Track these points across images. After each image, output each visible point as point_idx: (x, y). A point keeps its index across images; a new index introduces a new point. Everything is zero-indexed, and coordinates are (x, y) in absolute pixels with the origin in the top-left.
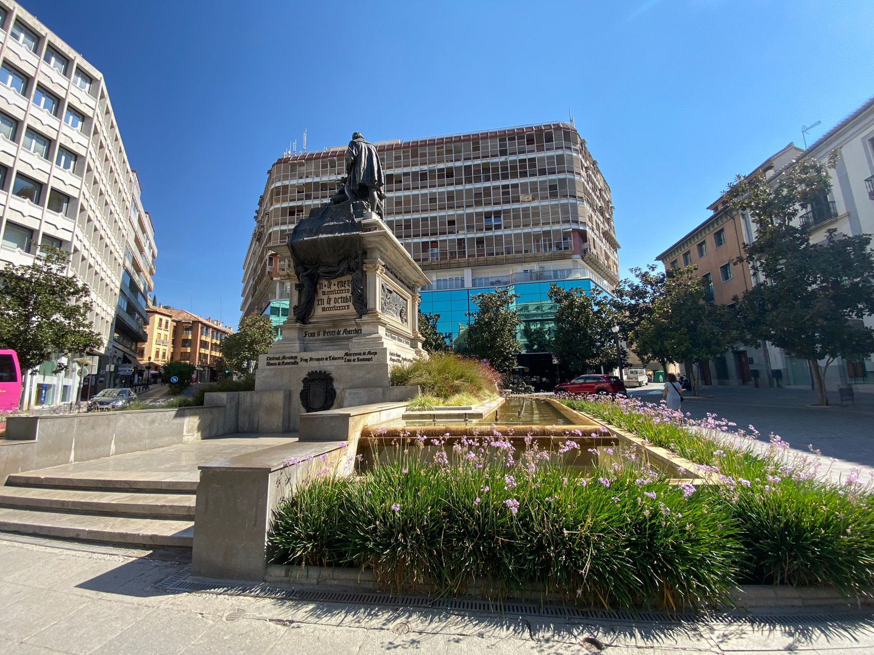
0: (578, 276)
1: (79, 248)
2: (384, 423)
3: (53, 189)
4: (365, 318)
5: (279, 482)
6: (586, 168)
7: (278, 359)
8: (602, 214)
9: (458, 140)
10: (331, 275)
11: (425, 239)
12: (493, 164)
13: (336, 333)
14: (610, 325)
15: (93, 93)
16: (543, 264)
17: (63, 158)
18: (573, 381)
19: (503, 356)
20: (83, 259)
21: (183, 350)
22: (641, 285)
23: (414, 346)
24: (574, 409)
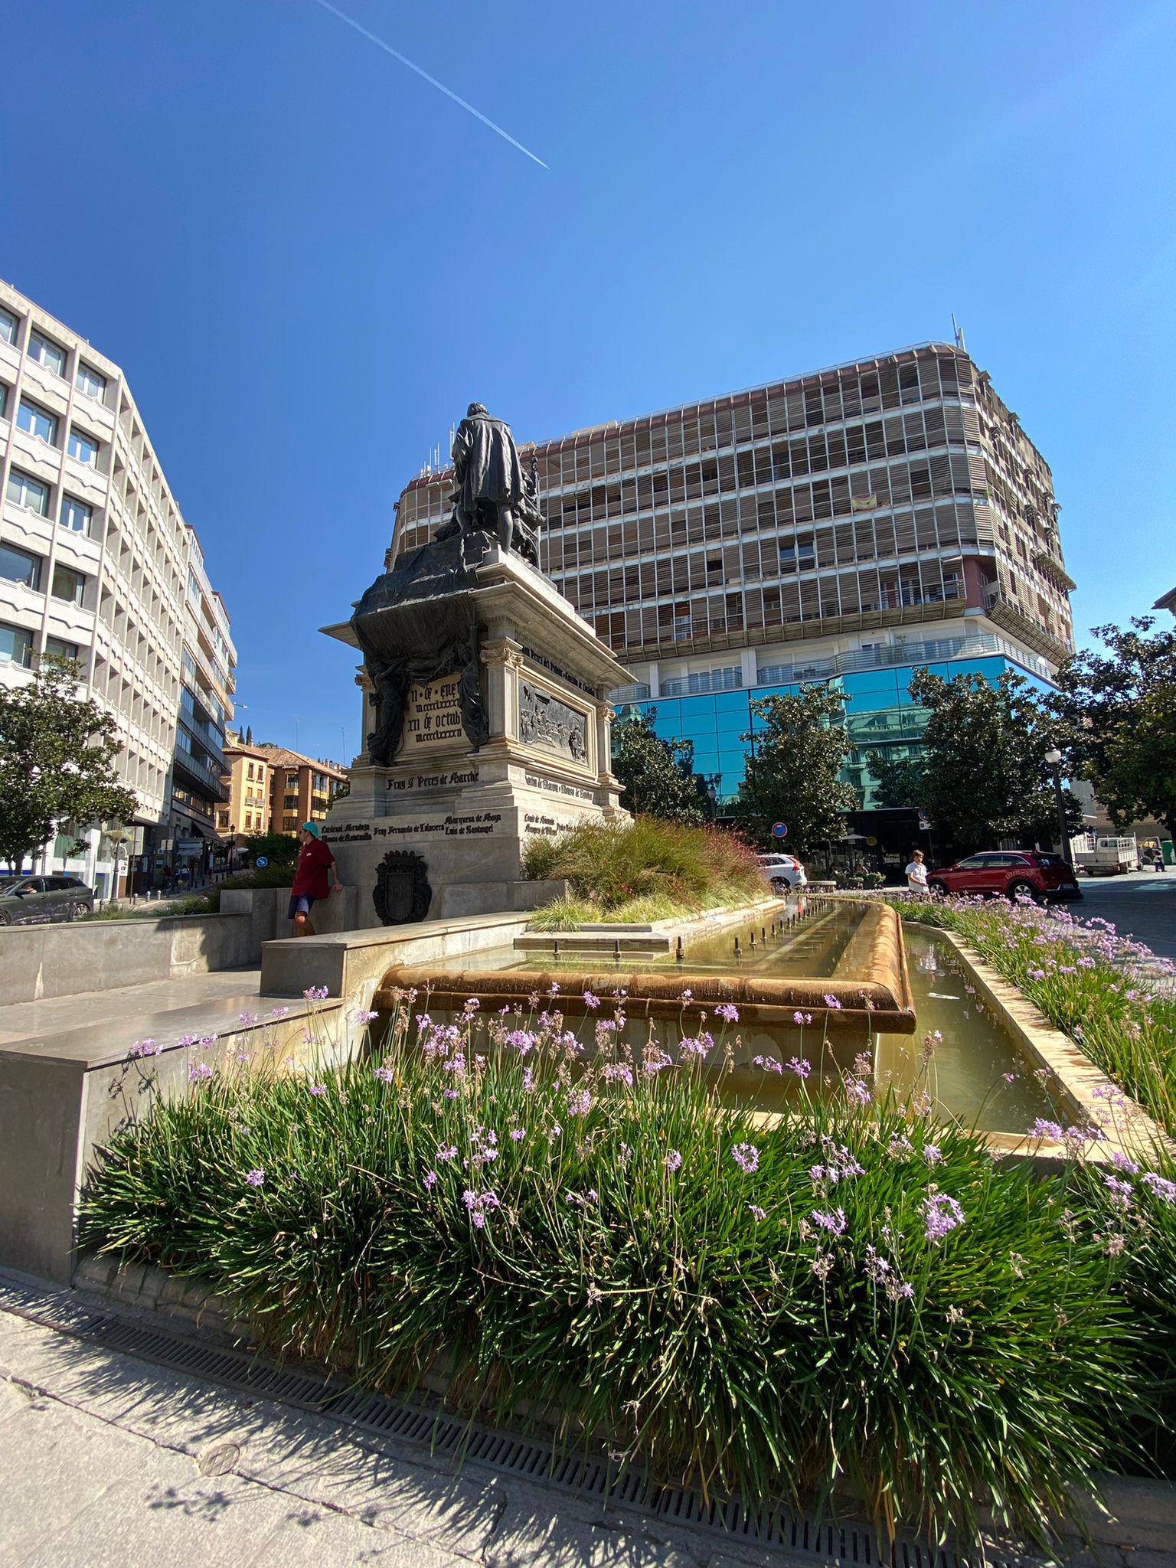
0: (980, 650)
1: (105, 656)
2: (451, 958)
3: (58, 565)
4: (484, 751)
5: (116, 1088)
6: (992, 430)
7: (339, 829)
8: (1032, 522)
9: (726, 405)
10: (429, 674)
11: (665, 601)
12: (793, 443)
13: (440, 781)
14: (1043, 748)
15: (108, 402)
16: (902, 631)
17: (72, 512)
18: (960, 865)
19: (817, 815)
20: (113, 673)
21: (286, 813)
22: (1117, 661)
23: (601, 800)
24: (937, 925)
